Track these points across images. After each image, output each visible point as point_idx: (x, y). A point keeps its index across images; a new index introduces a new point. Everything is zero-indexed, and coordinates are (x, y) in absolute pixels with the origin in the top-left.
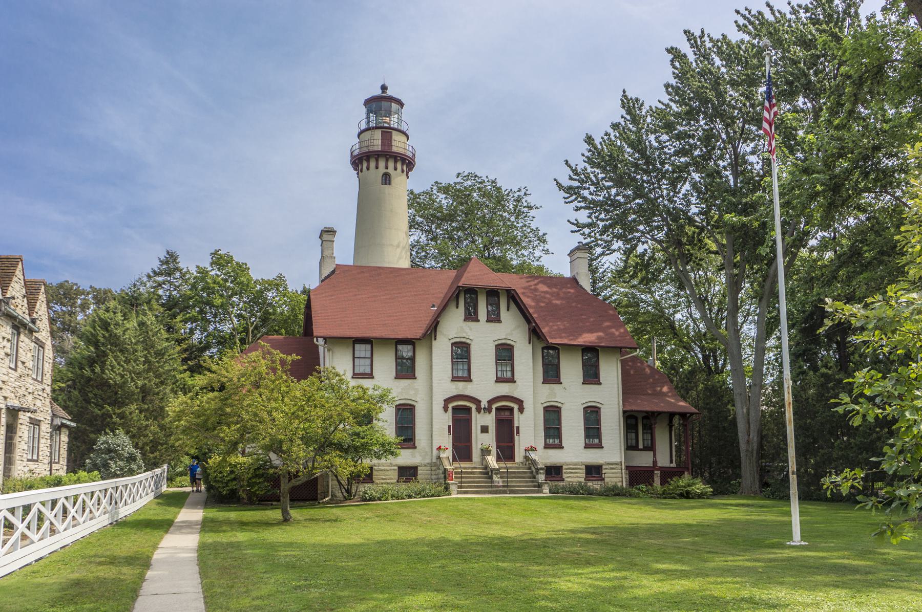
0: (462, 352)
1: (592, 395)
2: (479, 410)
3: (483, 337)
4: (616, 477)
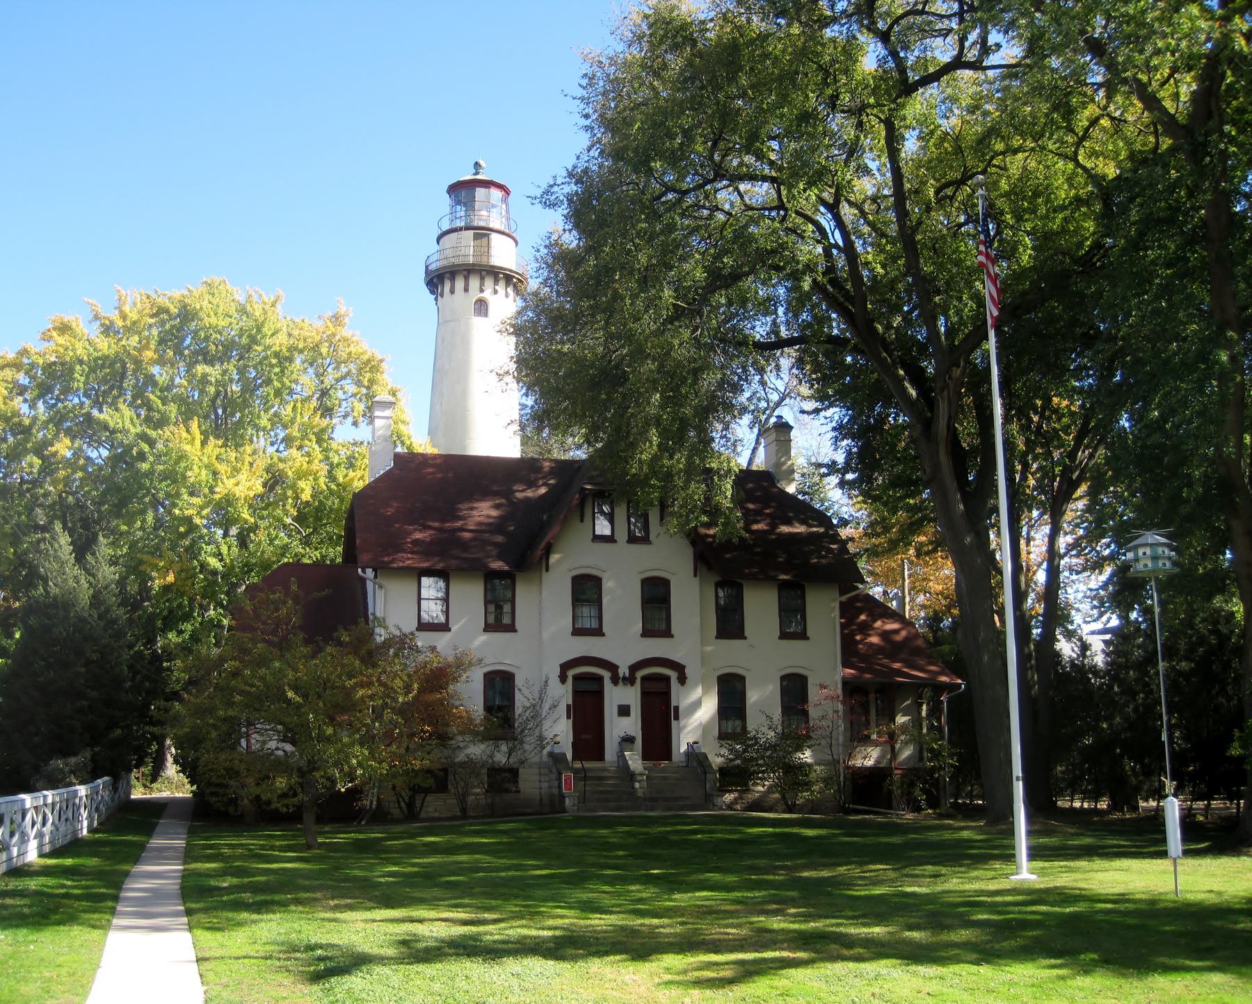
1: (794, 656)
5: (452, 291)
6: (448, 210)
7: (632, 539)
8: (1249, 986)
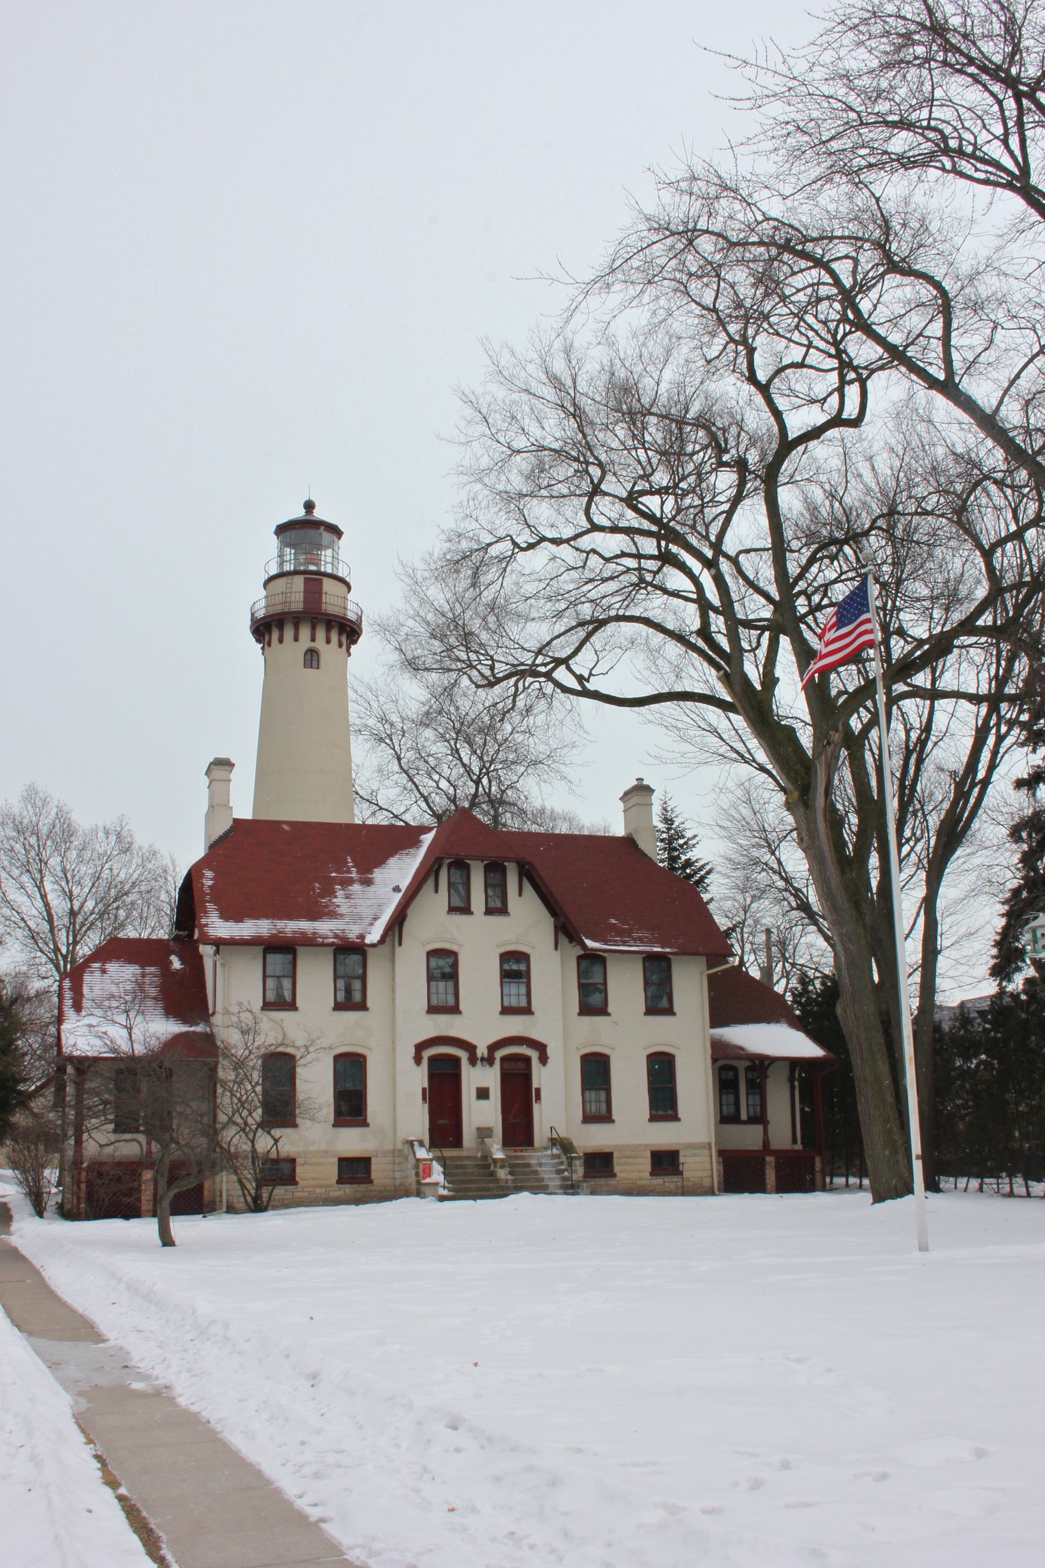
0: (444, 967)
1: (661, 1034)
2: (473, 1061)
3: (477, 942)
4: (699, 1165)
5: (281, 641)
6: (275, 553)
7: (489, 911)
8: (1037, 1188)
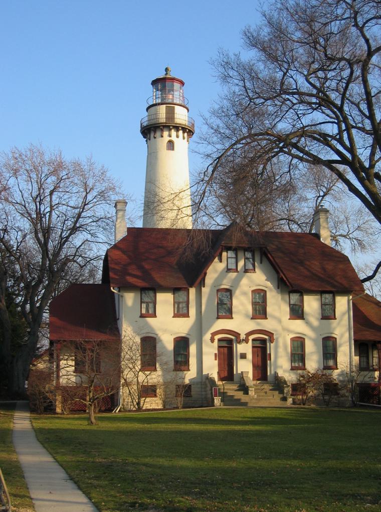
1: (298, 326)
